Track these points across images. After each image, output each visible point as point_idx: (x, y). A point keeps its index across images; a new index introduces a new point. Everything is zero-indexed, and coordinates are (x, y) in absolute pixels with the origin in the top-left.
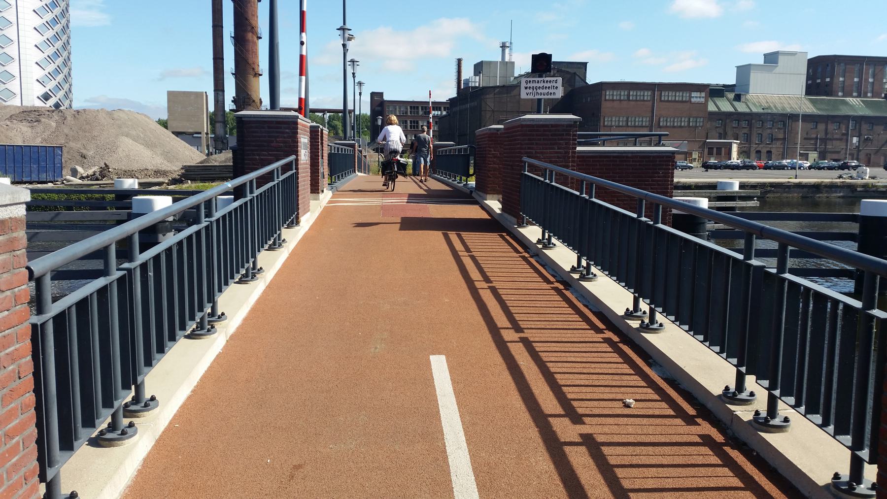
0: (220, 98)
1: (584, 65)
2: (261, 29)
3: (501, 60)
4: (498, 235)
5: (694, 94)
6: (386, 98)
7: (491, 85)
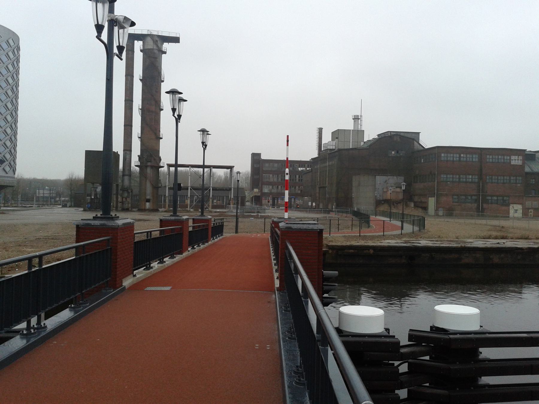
0: (128, 157)
1: (418, 134)
2: (163, 103)
3: (353, 129)
5: (513, 157)
6: (263, 157)
7: (346, 148)
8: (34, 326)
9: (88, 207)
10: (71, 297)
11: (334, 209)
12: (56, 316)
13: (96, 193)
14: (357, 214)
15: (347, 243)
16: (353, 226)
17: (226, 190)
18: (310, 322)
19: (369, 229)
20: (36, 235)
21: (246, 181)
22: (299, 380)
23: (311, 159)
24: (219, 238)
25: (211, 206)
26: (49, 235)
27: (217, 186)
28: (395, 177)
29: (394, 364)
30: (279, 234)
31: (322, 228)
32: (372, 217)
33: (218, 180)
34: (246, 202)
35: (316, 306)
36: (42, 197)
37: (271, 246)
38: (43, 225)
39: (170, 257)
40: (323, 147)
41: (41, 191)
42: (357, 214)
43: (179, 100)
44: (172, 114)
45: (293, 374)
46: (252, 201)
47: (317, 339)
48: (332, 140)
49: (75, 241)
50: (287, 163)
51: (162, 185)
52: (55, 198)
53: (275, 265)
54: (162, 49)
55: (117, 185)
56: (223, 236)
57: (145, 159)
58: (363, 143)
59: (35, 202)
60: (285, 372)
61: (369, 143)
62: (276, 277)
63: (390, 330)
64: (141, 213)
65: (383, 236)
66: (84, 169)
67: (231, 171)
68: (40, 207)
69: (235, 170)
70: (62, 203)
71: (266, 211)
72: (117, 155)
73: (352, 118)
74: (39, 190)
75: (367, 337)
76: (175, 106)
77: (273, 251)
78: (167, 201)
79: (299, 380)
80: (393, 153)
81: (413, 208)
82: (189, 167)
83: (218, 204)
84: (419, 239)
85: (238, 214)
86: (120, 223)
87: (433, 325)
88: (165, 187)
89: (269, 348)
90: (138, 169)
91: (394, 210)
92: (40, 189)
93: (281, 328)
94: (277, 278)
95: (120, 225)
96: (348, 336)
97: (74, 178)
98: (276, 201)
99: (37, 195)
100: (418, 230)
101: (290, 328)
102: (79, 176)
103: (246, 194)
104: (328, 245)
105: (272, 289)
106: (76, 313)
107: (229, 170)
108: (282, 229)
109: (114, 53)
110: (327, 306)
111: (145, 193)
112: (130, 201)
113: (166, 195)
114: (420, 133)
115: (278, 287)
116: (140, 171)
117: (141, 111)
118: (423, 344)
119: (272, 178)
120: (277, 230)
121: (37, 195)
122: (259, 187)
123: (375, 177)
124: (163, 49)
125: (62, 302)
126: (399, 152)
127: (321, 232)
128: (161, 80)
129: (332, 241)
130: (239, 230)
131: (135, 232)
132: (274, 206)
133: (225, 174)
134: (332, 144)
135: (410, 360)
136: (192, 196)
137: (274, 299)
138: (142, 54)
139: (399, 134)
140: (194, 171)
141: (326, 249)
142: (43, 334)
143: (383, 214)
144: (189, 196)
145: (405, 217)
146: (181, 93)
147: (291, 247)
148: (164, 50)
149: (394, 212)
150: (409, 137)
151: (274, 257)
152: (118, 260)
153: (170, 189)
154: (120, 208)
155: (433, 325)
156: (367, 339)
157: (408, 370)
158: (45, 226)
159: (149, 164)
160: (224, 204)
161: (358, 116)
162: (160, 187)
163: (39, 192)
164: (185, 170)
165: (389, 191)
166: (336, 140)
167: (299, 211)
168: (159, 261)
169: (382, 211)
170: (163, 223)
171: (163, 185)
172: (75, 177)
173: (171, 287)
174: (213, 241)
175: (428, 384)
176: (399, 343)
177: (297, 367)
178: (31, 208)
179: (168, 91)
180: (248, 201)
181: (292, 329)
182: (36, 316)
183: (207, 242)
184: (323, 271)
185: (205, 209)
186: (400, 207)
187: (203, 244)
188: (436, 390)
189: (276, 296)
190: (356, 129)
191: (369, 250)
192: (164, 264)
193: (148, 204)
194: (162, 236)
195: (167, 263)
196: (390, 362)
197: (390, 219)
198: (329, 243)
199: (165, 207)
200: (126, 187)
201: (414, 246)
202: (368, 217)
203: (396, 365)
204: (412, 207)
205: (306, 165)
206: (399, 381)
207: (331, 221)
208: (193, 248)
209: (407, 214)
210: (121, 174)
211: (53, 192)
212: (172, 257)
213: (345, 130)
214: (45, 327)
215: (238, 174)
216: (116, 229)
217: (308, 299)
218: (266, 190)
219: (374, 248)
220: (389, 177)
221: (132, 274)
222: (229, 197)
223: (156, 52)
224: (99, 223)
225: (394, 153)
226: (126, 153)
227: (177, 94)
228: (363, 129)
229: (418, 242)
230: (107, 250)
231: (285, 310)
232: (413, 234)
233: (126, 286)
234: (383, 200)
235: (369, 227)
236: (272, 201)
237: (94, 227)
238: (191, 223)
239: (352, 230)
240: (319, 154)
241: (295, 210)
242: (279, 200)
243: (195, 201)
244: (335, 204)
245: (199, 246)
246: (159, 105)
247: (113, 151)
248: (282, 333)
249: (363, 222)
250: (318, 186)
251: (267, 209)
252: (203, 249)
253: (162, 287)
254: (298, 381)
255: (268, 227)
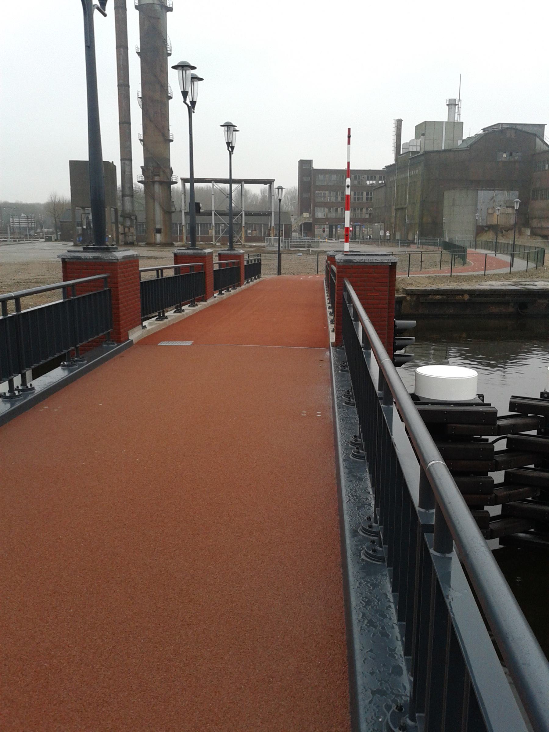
0: (127, 169)
3: (447, 121)
4: (448, 251)
6: (316, 166)
7: (436, 149)
8: (18, 387)
9: (79, 241)
10: (63, 353)
11: (416, 240)
12: (45, 376)
13: (89, 222)
14: (449, 246)
15: (433, 286)
16: (442, 263)
17: (265, 215)
18: (371, 377)
19: (466, 267)
20: (15, 278)
21: (291, 201)
22: (357, 452)
23: (385, 166)
24: (255, 281)
25: (244, 238)
26: (31, 278)
27: (251, 209)
28: (506, 192)
29: (487, 440)
30: (335, 272)
31: (396, 261)
32: (470, 250)
33: (252, 201)
34: (292, 232)
35: (378, 355)
36: (18, 228)
37: (326, 291)
38: (23, 265)
39: (190, 304)
40: (403, 149)
41: (16, 220)
42: (449, 246)
43: (192, 78)
44: (182, 99)
45: (349, 445)
46: (301, 230)
47: (378, 396)
48: (415, 139)
49: (62, 281)
50: (348, 172)
51: (175, 209)
52: (35, 229)
53: (329, 308)
54: (167, 4)
55: (116, 210)
56: (261, 279)
57: (150, 171)
58: (461, 141)
59: (9, 235)
60: (339, 444)
61: (470, 143)
62: (332, 330)
63: (485, 397)
64: (150, 249)
65: (484, 276)
66: (70, 187)
67: (270, 187)
68: (16, 241)
69: (276, 185)
70: (45, 236)
71: (321, 244)
72: (111, 166)
73: (446, 104)
74: (13, 218)
75: (452, 405)
76: (187, 85)
77: (328, 297)
78: (184, 231)
79: (358, 452)
80: (505, 155)
81: (529, 237)
82: (211, 183)
83: (254, 235)
84: (536, 280)
85: (281, 249)
86: (119, 256)
87: (545, 391)
88: (181, 211)
89: (320, 416)
90: (142, 186)
91: (502, 240)
92: (14, 217)
93: (337, 391)
94: (332, 331)
95: (119, 258)
96: (427, 404)
97: (57, 200)
98: (334, 230)
99: (12, 226)
100: (535, 268)
101: (348, 391)
102: (63, 197)
103: (293, 220)
104: (405, 289)
105: (325, 345)
106: (70, 371)
107: (268, 185)
108: (338, 262)
109: (94, 5)
110: (400, 366)
111: (154, 220)
112: (135, 232)
113: (182, 223)
114: (546, 126)
115: (334, 342)
116: (145, 189)
117: (142, 101)
118: (529, 415)
119: (330, 197)
120: (333, 266)
121: (12, 226)
122: (310, 211)
123: (477, 192)
124: (168, 4)
125: (51, 358)
126: (514, 154)
127: (393, 267)
128: (167, 52)
129: (411, 284)
130: (282, 270)
131: (140, 269)
132: (332, 237)
133: (263, 192)
134: (416, 145)
135: (510, 436)
136: (217, 225)
137: (328, 357)
138: (137, 12)
139: (515, 127)
140: (219, 188)
141: (404, 295)
142: (30, 397)
143: (487, 246)
144: (213, 224)
145: (517, 249)
146: (194, 68)
147: (351, 286)
148: (169, 5)
149: (502, 242)
150: (529, 131)
151: (330, 305)
152: (121, 305)
153: (186, 214)
154: (122, 241)
155: (545, 391)
156: (452, 408)
157: (507, 448)
158: (25, 266)
159: (157, 178)
160: (262, 235)
161: (455, 100)
162: (174, 212)
163: (13, 220)
164: (206, 188)
165: (496, 213)
166: (423, 137)
167: (366, 243)
168: (176, 310)
169: (485, 241)
170: (177, 258)
171: (178, 209)
172: (59, 199)
173: (193, 342)
174: (247, 285)
175: (532, 466)
176: (496, 413)
177: (355, 437)
178: (5, 243)
179: (176, 64)
180: (295, 231)
181: (351, 393)
182: (20, 375)
183: (240, 285)
184: (395, 320)
185: (236, 243)
186: (511, 234)
187: (234, 288)
188: (543, 473)
189: (332, 353)
190: (452, 120)
191: (463, 295)
192: (183, 313)
193: (158, 235)
194: (178, 276)
195: (186, 311)
196: (483, 437)
197: (496, 252)
198: (407, 287)
199: (181, 240)
200: (128, 212)
201: (526, 288)
202: (464, 250)
203: (490, 441)
204: (528, 236)
205: (378, 177)
206: (494, 460)
207: (411, 255)
208: (221, 293)
209: (520, 245)
210: (119, 194)
211: (31, 221)
212: (193, 304)
213: (435, 122)
214: (33, 389)
215: (280, 190)
216: (112, 265)
217: (370, 350)
218: (320, 214)
219: (471, 293)
220: (496, 192)
221: (141, 325)
222: (268, 224)
223: (158, 8)
224: (92, 256)
225: (505, 156)
226: (124, 163)
227: (188, 70)
228: (461, 121)
229: (532, 283)
230: (105, 291)
231: (341, 370)
232: (527, 273)
233: (133, 341)
234: (487, 226)
235: (464, 263)
236: (328, 230)
237: (85, 261)
238: (216, 260)
239: (440, 269)
240: (397, 159)
241: (361, 243)
242: (339, 229)
243: (222, 232)
244: (418, 232)
245: (228, 291)
246: (166, 91)
247: (105, 159)
248: (338, 398)
249: (457, 258)
250: (394, 207)
251: (321, 242)
252: (234, 296)
253: (181, 342)
254: (356, 453)
255: (323, 268)
